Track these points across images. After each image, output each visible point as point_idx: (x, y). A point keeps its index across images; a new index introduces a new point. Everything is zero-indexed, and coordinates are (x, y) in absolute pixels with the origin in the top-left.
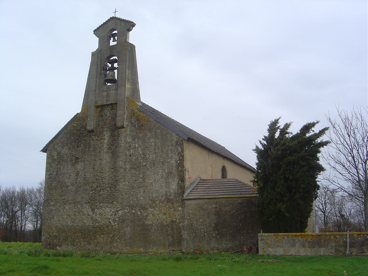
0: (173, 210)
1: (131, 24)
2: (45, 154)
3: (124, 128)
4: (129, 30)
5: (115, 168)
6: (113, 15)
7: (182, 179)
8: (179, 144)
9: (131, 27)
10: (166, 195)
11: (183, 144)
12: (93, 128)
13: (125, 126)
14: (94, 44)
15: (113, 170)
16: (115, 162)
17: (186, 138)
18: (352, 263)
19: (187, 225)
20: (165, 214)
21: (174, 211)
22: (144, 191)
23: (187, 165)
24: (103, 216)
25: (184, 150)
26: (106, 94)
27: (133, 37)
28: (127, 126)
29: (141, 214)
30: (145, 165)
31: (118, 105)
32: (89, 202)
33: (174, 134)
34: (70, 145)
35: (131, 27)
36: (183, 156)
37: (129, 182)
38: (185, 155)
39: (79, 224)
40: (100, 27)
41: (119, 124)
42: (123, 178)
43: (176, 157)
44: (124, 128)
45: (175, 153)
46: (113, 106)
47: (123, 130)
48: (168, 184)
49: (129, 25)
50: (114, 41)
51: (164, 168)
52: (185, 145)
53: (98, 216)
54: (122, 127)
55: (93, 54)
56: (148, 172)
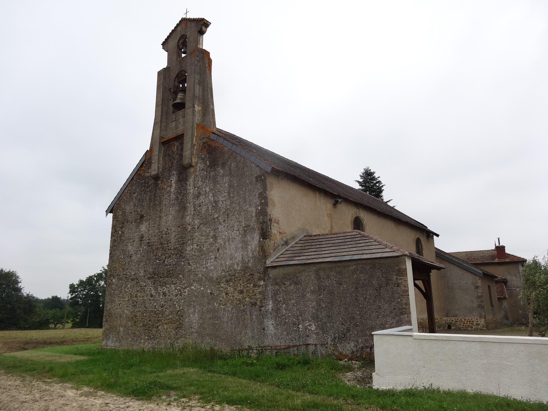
0: (252, 285)
1: (202, 23)
2: (111, 215)
3: (193, 167)
4: (202, 33)
5: (182, 228)
6: (184, 17)
7: (265, 235)
8: (261, 179)
9: (203, 28)
10: (243, 260)
11: (265, 179)
12: (158, 173)
13: (194, 164)
14: (161, 59)
15: (179, 229)
16: (183, 217)
17: (269, 169)
18: (463, 399)
19: (272, 309)
20: (241, 292)
21: (253, 286)
22: (216, 258)
23: (276, 212)
24: (167, 297)
25: (268, 189)
26: (174, 125)
27: (208, 42)
28: (197, 163)
29: (211, 293)
30: (217, 218)
31: (185, 135)
32: (153, 277)
33: (254, 165)
34: (138, 200)
35: (203, 28)
36: (266, 198)
37: (197, 245)
38: (269, 197)
39: (140, 309)
40: (168, 37)
41: (186, 162)
42: (190, 240)
43: (257, 201)
44: (193, 167)
45: (255, 195)
46: (180, 138)
47: (192, 170)
48: (245, 244)
49: (201, 25)
50: (402, 258)
51: (241, 220)
52: (271, 181)
53: (161, 297)
54: (191, 166)
55: (159, 73)
56: (220, 227)
